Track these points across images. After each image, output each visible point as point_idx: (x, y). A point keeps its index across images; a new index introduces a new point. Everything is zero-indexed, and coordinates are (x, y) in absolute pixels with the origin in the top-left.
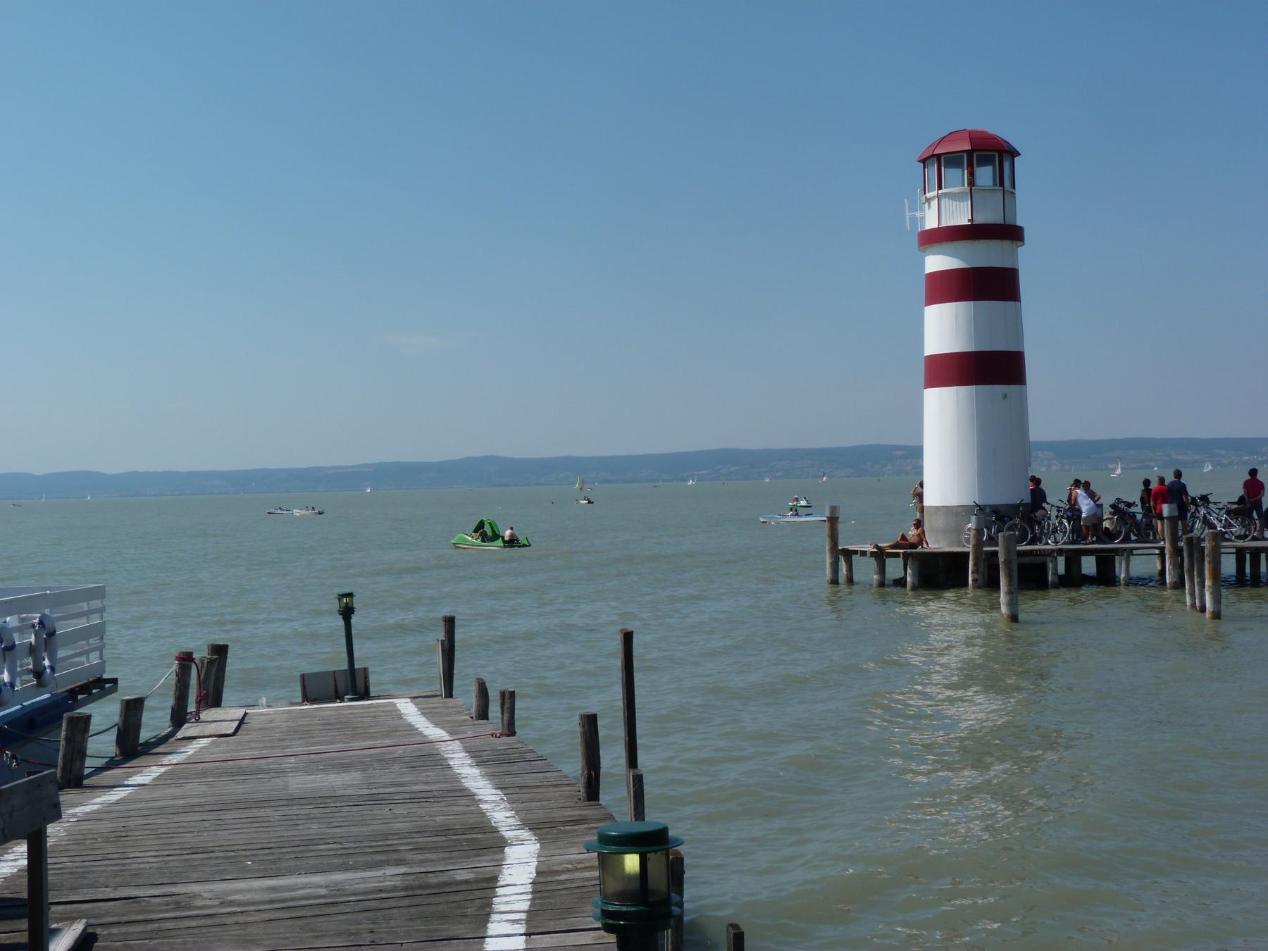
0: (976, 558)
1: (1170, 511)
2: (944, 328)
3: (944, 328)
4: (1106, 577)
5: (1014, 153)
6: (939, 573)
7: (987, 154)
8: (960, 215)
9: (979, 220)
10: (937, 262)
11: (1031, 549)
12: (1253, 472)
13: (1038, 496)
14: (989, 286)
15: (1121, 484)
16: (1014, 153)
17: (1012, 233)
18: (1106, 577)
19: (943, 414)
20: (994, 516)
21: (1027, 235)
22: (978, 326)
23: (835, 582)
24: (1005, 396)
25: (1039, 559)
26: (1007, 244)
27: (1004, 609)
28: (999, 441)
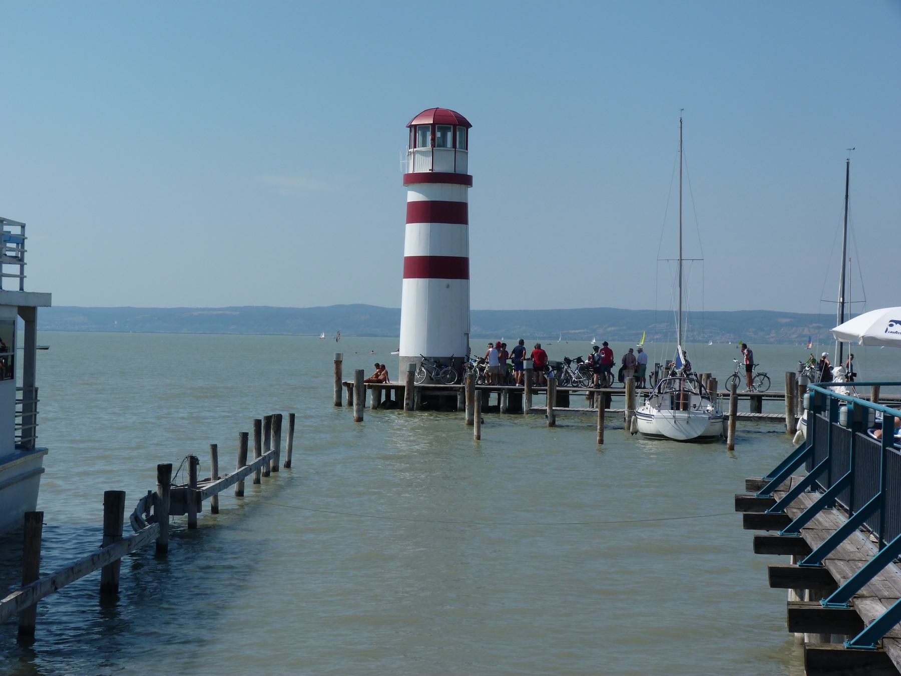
0: (408, 390)
1: (527, 364)
2: (415, 240)
3: (415, 240)
4: (515, 408)
5: (468, 125)
6: (392, 401)
7: (448, 128)
8: (424, 166)
9: (437, 169)
10: (414, 196)
11: (441, 388)
12: (522, 342)
13: (608, 352)
14: (446, 213)
15: (584, 349)
16: (468, 125)
17: (465, 180)
18: (515, 408)
19: (412, 294)
20: (438, 365)
21: (474, 181)
22: (432, 239)
23: (339, 404)
24: (448, 286)
25: (452, 393)
26: (456, 187)
27: (355, 414)
28: (448, 316)
